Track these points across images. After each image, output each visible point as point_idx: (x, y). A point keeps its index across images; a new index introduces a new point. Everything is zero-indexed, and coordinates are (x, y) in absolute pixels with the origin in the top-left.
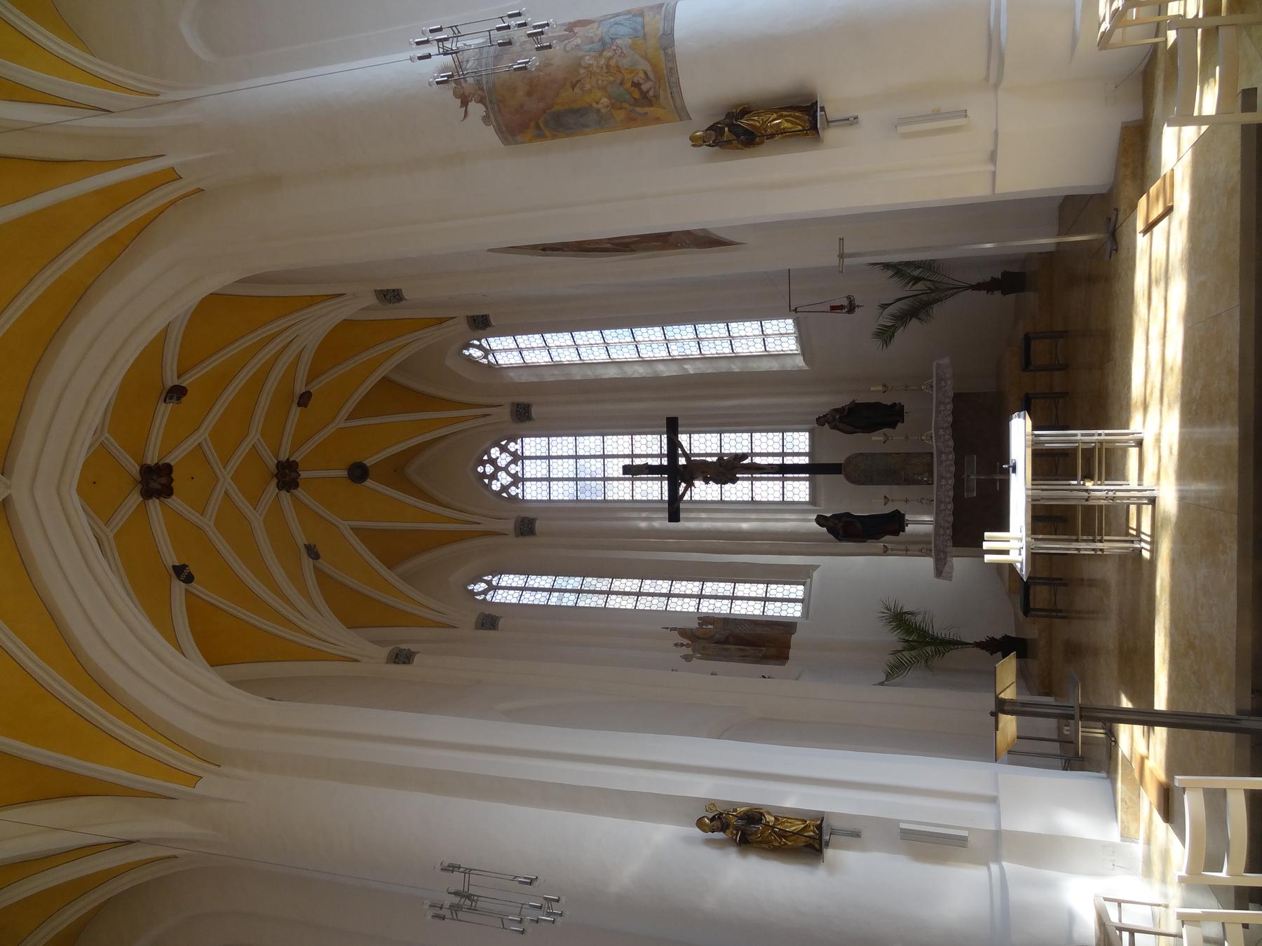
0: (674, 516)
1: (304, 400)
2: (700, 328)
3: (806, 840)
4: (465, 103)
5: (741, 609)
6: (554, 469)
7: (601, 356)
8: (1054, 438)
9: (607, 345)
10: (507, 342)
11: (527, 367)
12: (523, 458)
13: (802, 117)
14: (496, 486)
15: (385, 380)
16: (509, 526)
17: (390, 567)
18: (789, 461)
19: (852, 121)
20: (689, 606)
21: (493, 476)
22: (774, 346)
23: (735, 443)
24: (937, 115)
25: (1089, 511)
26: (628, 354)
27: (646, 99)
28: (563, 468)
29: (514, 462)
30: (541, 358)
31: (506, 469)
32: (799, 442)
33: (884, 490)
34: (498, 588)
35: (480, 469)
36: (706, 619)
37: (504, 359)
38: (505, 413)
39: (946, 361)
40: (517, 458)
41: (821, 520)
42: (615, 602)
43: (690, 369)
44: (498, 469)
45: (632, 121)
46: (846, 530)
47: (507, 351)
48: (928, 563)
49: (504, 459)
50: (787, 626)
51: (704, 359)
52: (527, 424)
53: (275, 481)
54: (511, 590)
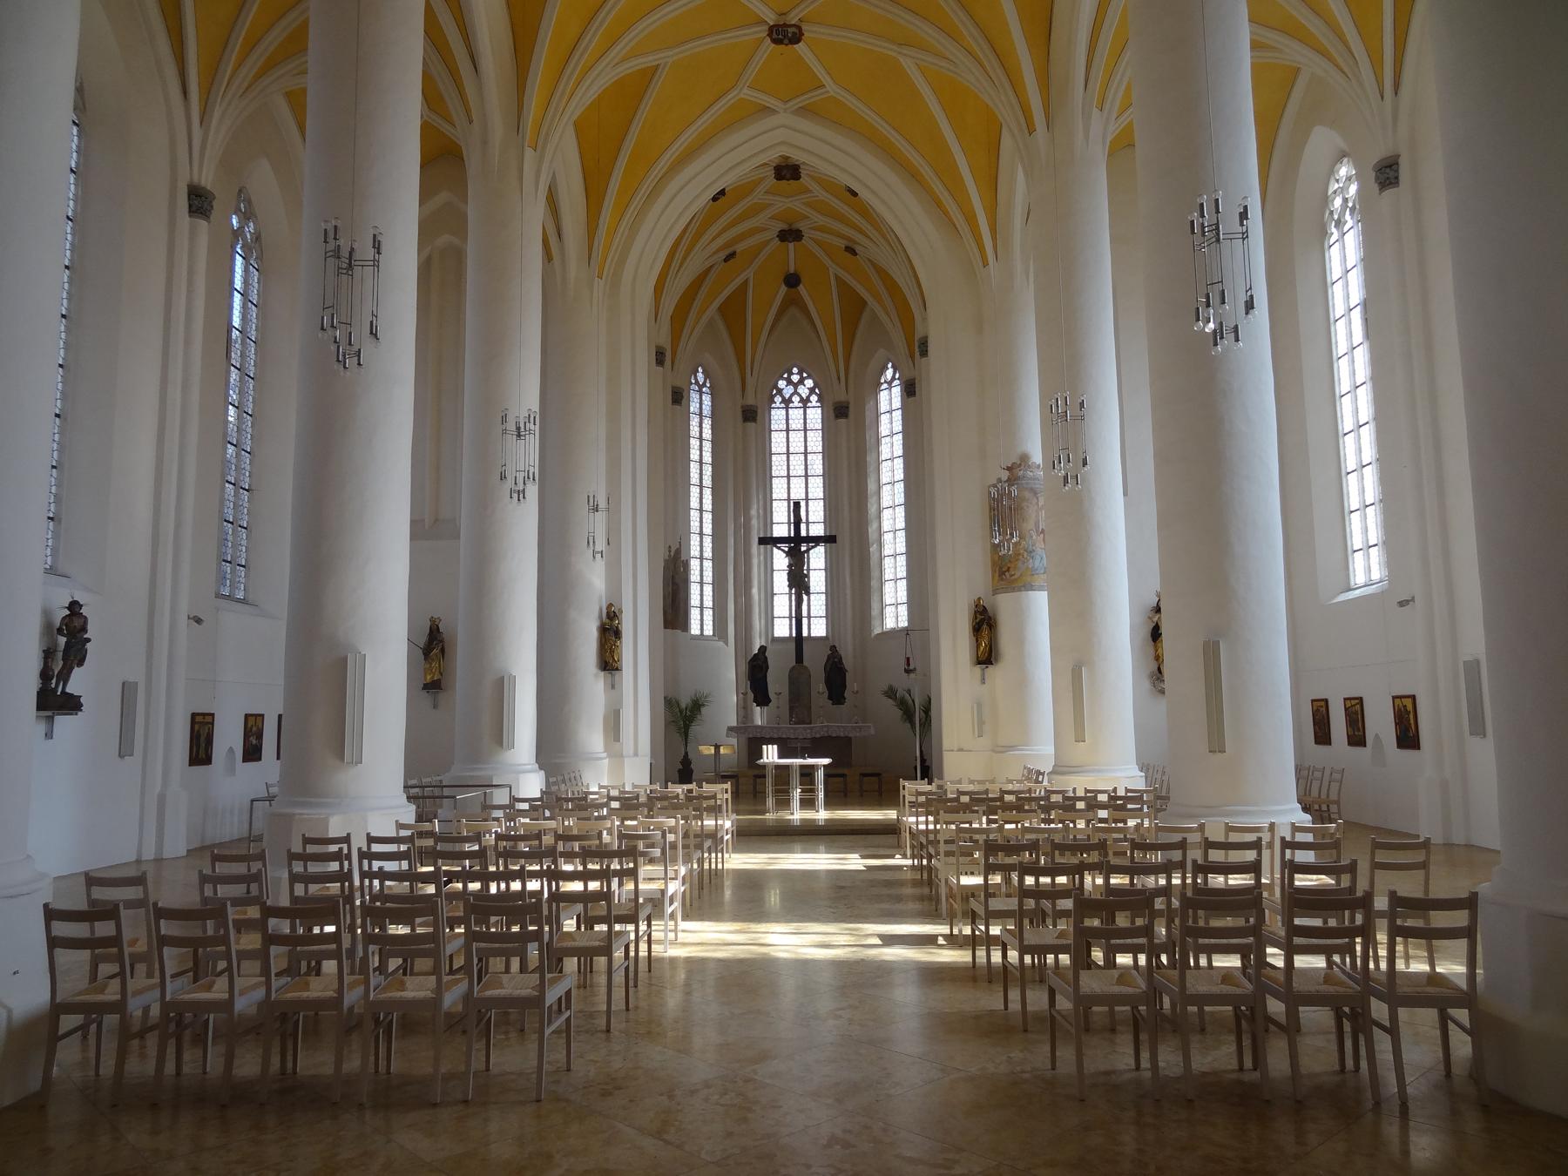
0: (763, 541)
1: (851, 250)
2: (903, 558)
3: (608, 663)
4: (1009, 469)
5: (694, 590)
6: (796, 435)
7: (885, 478)
8: (820, 775)
9: (893, 483)
10: (897, 403)
11: (877, 415)
12: (805, 408)
13: (987, 657)
14: (782, 384)
15: (864, 303)
16: (750, 401)
17: (720, 309)
18: (805, 621)
19: (983, 681)
20: (695, 551)
21: (789, 382)
22: (889, 612)
23: (818, 581)
24: (981, 723)
25: (787, 792)
26: (886, 500)
27: (1002, 574)
28: (797, 440)
29: (802, 400)
30: (884, 429)
31: (796, 392)
32: (818, 629)
33: (786, 691)
34: (701, 393)
35: (795, 370)
36: (686, 565)
37: (883, 396)
38: (842, 397)
39: (872, 731)
40: (805, 402)
41: (763, 649)
42: (694, 491)
43: (873, 549)
44: (796, 386)
45: (994, 564)
46: (756, 670)
47: (890, 399)
48: (734, 723)
49: (803, 391)
50: (685, 626)
51: (881, 559)
52: (832, 413)
53: (785, 227)
54: (700, 403)
